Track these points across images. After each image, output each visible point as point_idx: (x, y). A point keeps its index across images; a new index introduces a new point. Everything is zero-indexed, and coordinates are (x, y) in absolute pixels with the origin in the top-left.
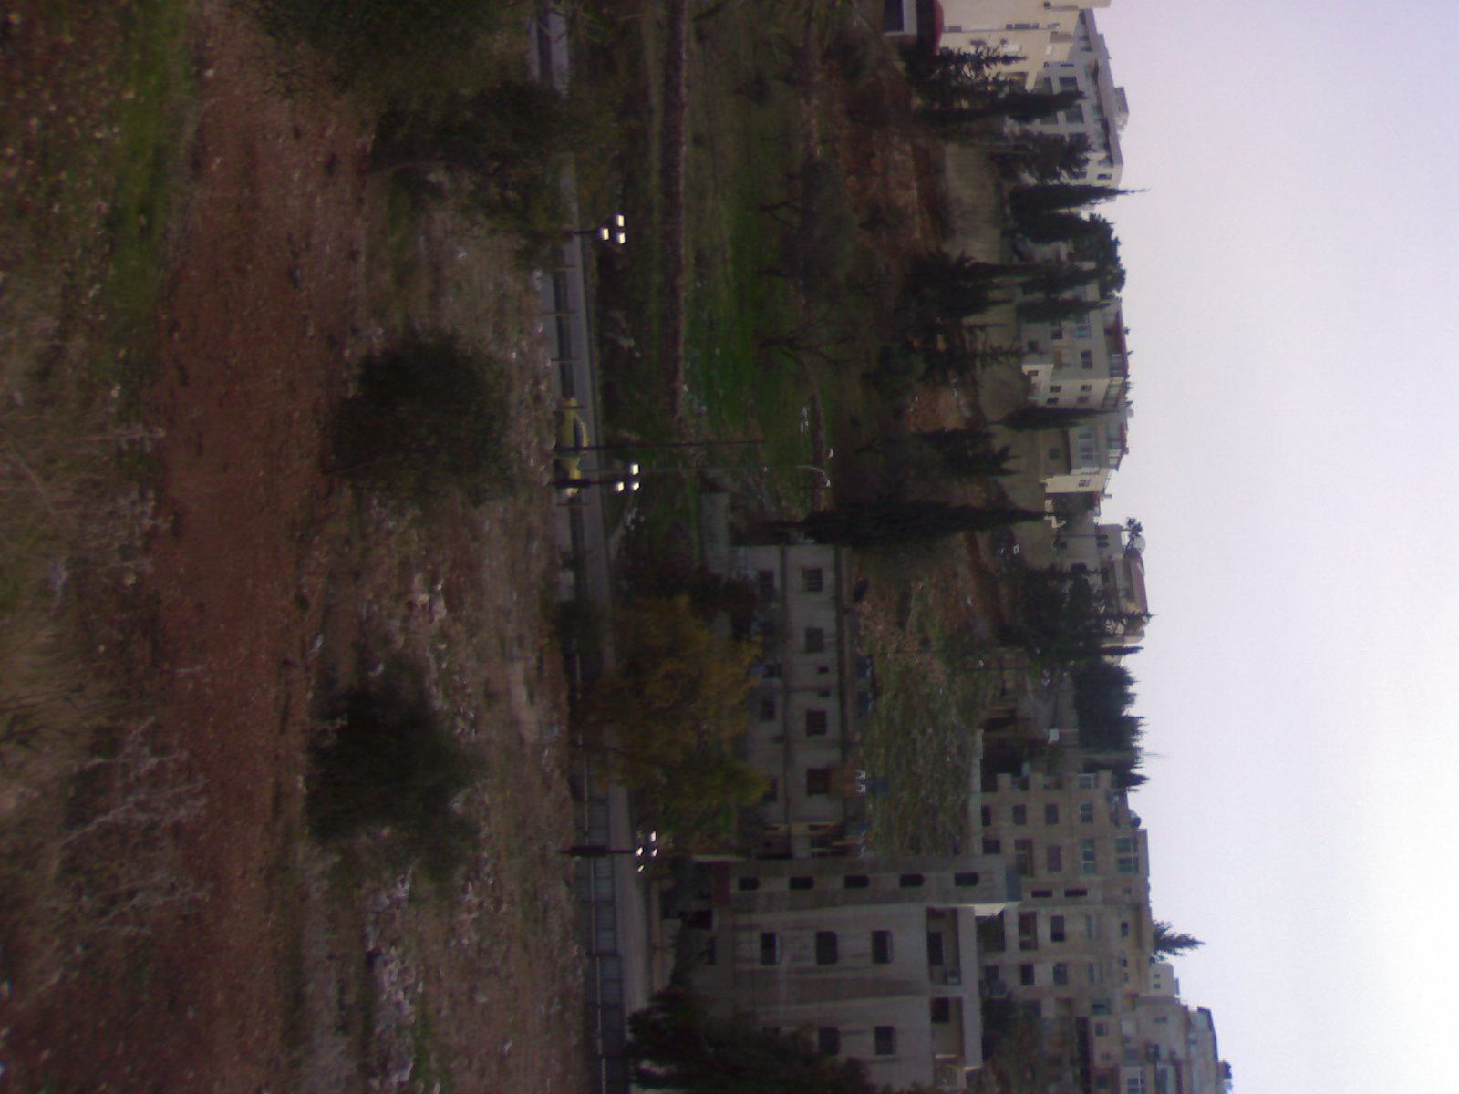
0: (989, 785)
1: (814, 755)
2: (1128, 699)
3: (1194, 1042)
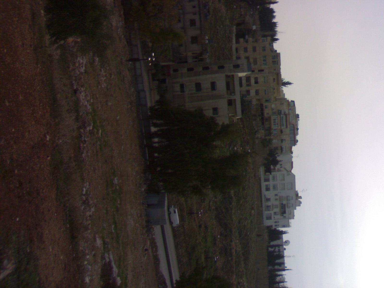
0: (237, 42)
1: (193, 32)
2: (274, 17)
3: (291, 109)
